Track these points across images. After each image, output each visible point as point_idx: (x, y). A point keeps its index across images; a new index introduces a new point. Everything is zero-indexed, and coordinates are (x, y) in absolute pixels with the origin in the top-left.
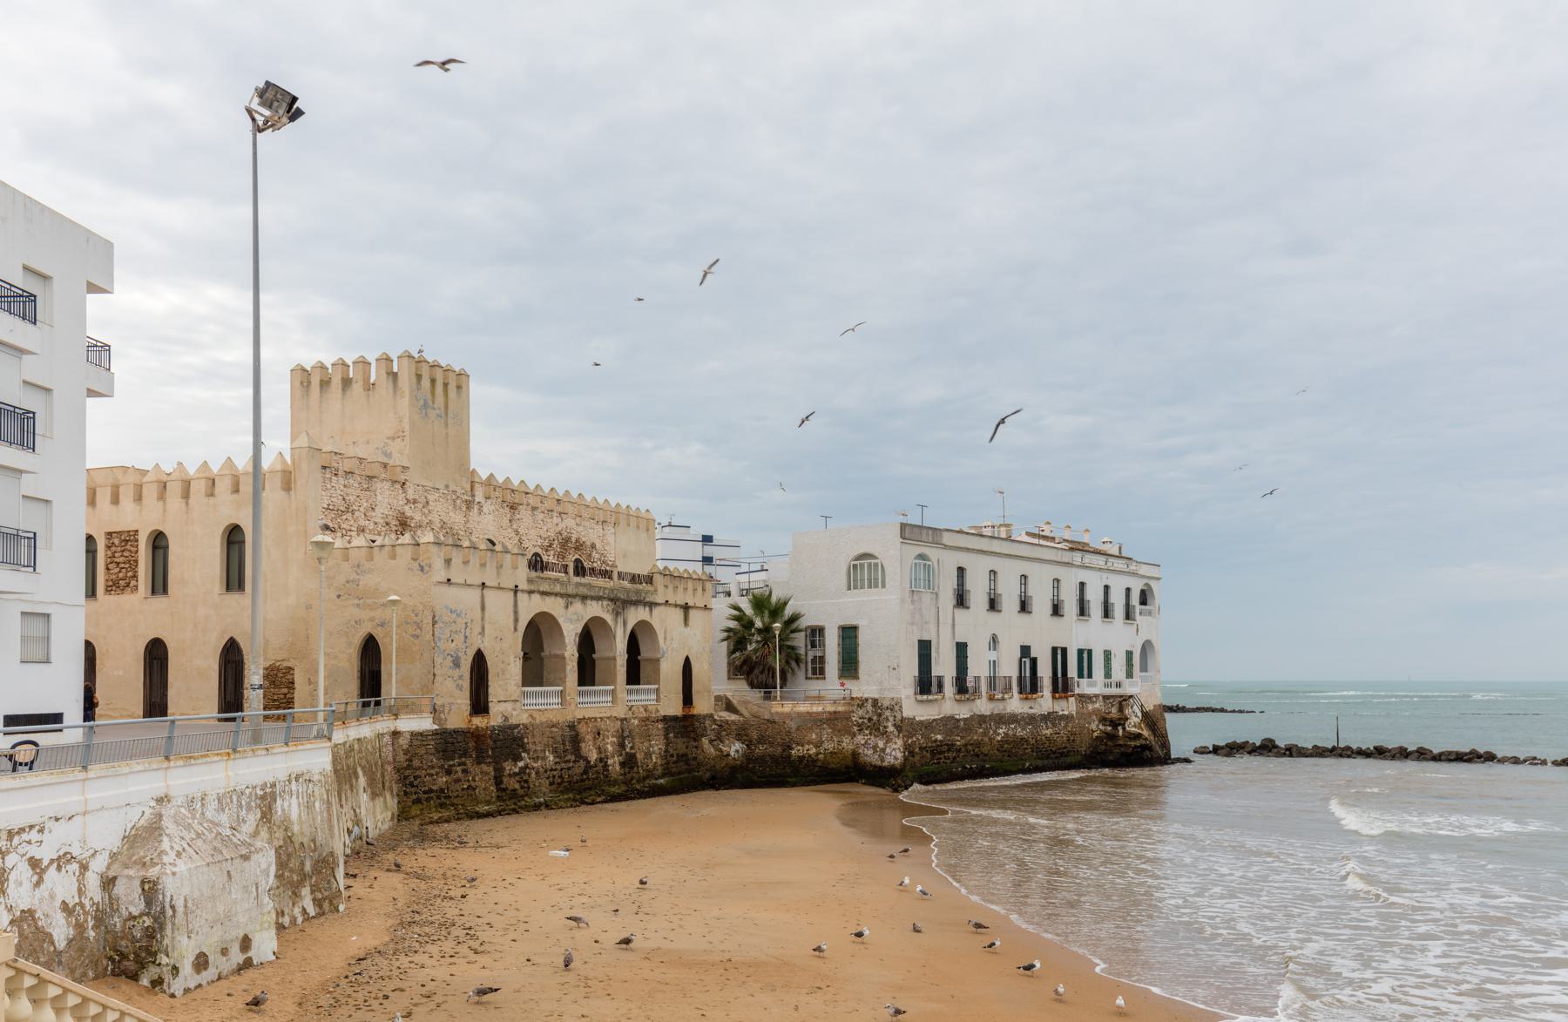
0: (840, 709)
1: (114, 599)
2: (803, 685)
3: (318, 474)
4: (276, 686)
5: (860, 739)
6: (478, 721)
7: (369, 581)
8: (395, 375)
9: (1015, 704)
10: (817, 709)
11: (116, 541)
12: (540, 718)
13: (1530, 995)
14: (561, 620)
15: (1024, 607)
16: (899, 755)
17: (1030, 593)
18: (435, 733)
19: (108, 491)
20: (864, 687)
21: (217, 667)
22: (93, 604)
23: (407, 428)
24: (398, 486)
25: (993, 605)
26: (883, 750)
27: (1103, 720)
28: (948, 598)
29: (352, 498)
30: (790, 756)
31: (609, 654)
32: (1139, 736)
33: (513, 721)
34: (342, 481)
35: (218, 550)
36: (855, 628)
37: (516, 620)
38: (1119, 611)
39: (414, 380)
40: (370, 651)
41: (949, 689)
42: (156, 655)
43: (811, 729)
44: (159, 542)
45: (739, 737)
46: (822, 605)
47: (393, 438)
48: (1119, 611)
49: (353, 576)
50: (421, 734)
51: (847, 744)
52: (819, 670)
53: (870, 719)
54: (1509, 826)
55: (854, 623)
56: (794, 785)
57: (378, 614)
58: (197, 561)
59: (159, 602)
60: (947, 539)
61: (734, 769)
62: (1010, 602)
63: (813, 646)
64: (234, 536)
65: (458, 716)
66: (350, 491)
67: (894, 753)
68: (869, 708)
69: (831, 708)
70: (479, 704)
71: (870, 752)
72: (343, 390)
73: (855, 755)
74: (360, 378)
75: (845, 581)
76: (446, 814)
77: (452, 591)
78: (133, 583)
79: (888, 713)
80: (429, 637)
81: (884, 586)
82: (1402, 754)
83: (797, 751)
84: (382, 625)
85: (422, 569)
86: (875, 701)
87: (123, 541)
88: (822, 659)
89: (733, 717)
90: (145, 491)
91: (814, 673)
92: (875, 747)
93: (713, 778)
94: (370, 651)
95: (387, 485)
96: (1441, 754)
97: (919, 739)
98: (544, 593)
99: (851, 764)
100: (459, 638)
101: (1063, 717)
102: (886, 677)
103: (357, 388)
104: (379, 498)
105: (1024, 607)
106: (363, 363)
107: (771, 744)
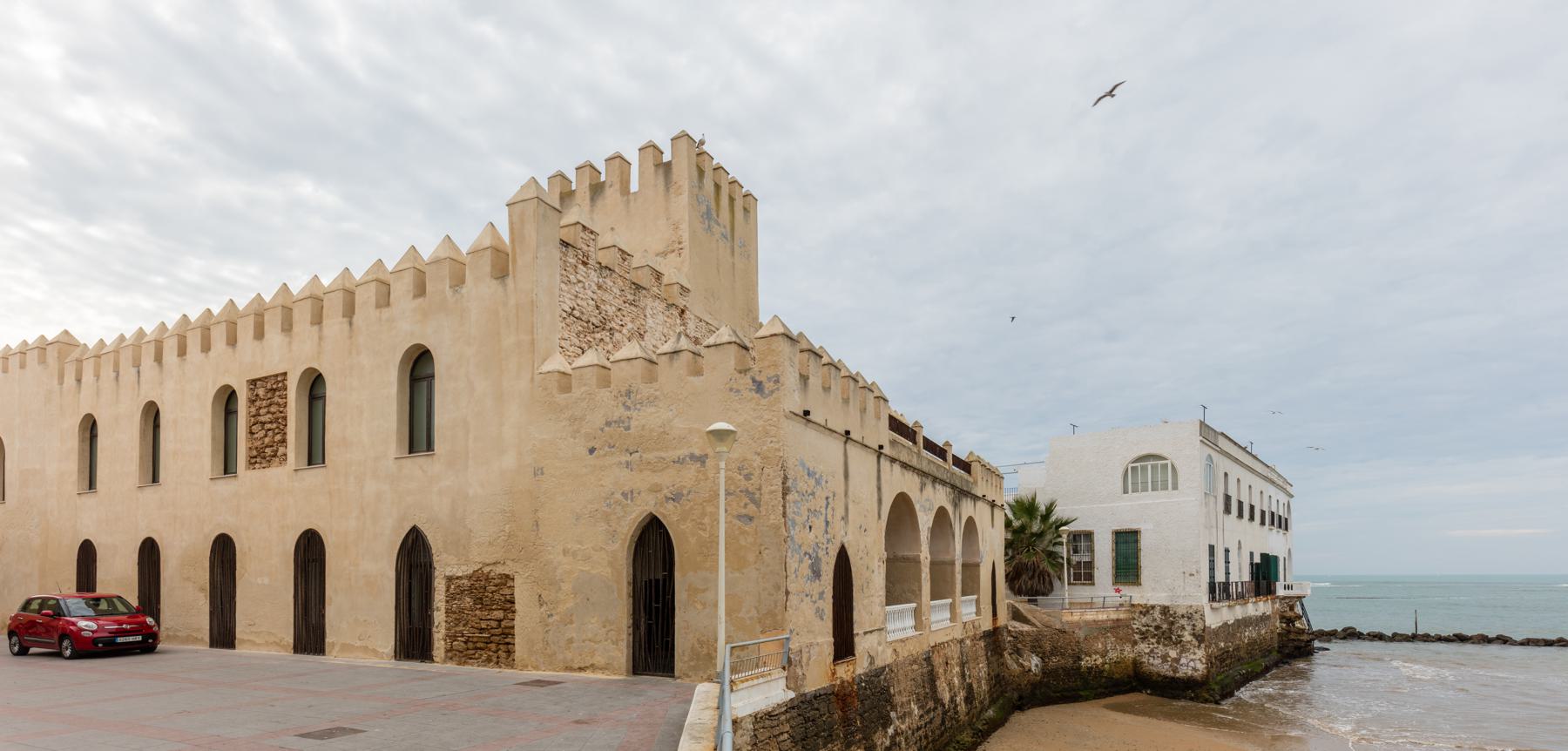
0: (1122, 616)
1: (258, 474)
2: (1067, 592)
3: (556, 253)
4: (484, 607)
5: (1143, 647)
6: (844, 672)
7: (647, 418)
8: (668, 166)
10: (1102, 617)
11: (261, 392)
12: (904, 653)
14: (917, 507)
16: (1201, 667)
18: (791, 706)
19: (250, 321)
20: (1152, 591)
21: (392, 574)
22: (226, 486)
23: (686, 236)
24: (676, 313)
26: (1177, 660)
29: (611, 310)
30: (1080, 667)
31: (948, 558)
33: (879, 663)
34: (594, 276)
35: (394, 390)
36: (1135, 534)
37: (880, 501)
39: (695, 173)
40: (653, 550)
42: (310, 553)
43: (1096, 638)
44: (315, 385)
45: (1034, 650)
46: (1094, 508)
47: (664, 254)
49: (620, 412)
50: (769, 715)
51: (1129, 653)
52: (1085, 574)
53: (1157, 628)
55: (1134, 527)
56: (1086, 699)
57: (667, 479)
58: (365, 409)
59: (315, 475)
60: (1222, 442)
61: (1035, 686)
63: (1076, 551)
64: (419, 366)
65: (819, 674)
66: (606, 297)
67: (1194, 663)
68: (1157, 614)
69: (1114, 616)
70: (844, 646)
71: (1157, 662)
72: (593, 199)
73: (1136, 664)
74: (616, 179)
75: (1120, 484)
77: (811, 435)
78: (281, 450)
79: (1183, 622)
80: (775, 518)
81: (1175, 487)
82: (1484, 640)
83: (1086, 662)
84: (676, 498)
85: (759, 387)
86: (1165, 610)
87: (269, 387)
88: (1090, 565)
89: (1026, 628)
90: (296, 315)
92: (1165, 658)
93: (1021, 698)
94: (653, 550)
95: (660, 306)
96: (1395, 635)
98: (905, 466)
99: (1130, 671)
100: (819, 523)
102: (1171, 582)
103: (612, 195)
104: (650, 321)
106: (618, 160)
107: (1063, 655)
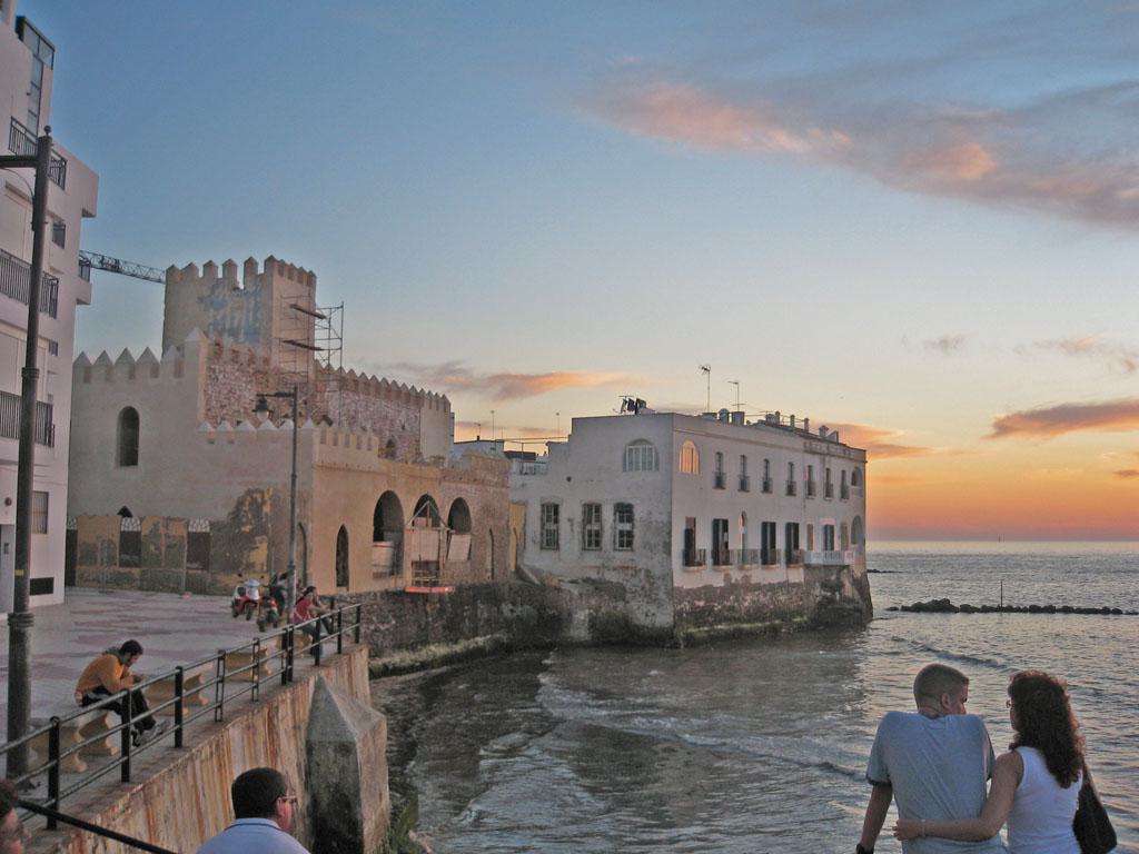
9: (759, 575)
13: (148, 619)
15: (766, 488)
17: (771, 476)
25: (743, 486)
27: (825, 586)
28: (711, 481)
32: (852, 601)
38: (837, 491)
41: (709, 560)
48: (837, 491)
54: (760, 625)
62: (756, 483)
76: (715, 749)
79: (659, 582)
88: (598, 534)
91: (621, 545)
97: (686, 606)
101: (794, 585)
105: (766, 488)
